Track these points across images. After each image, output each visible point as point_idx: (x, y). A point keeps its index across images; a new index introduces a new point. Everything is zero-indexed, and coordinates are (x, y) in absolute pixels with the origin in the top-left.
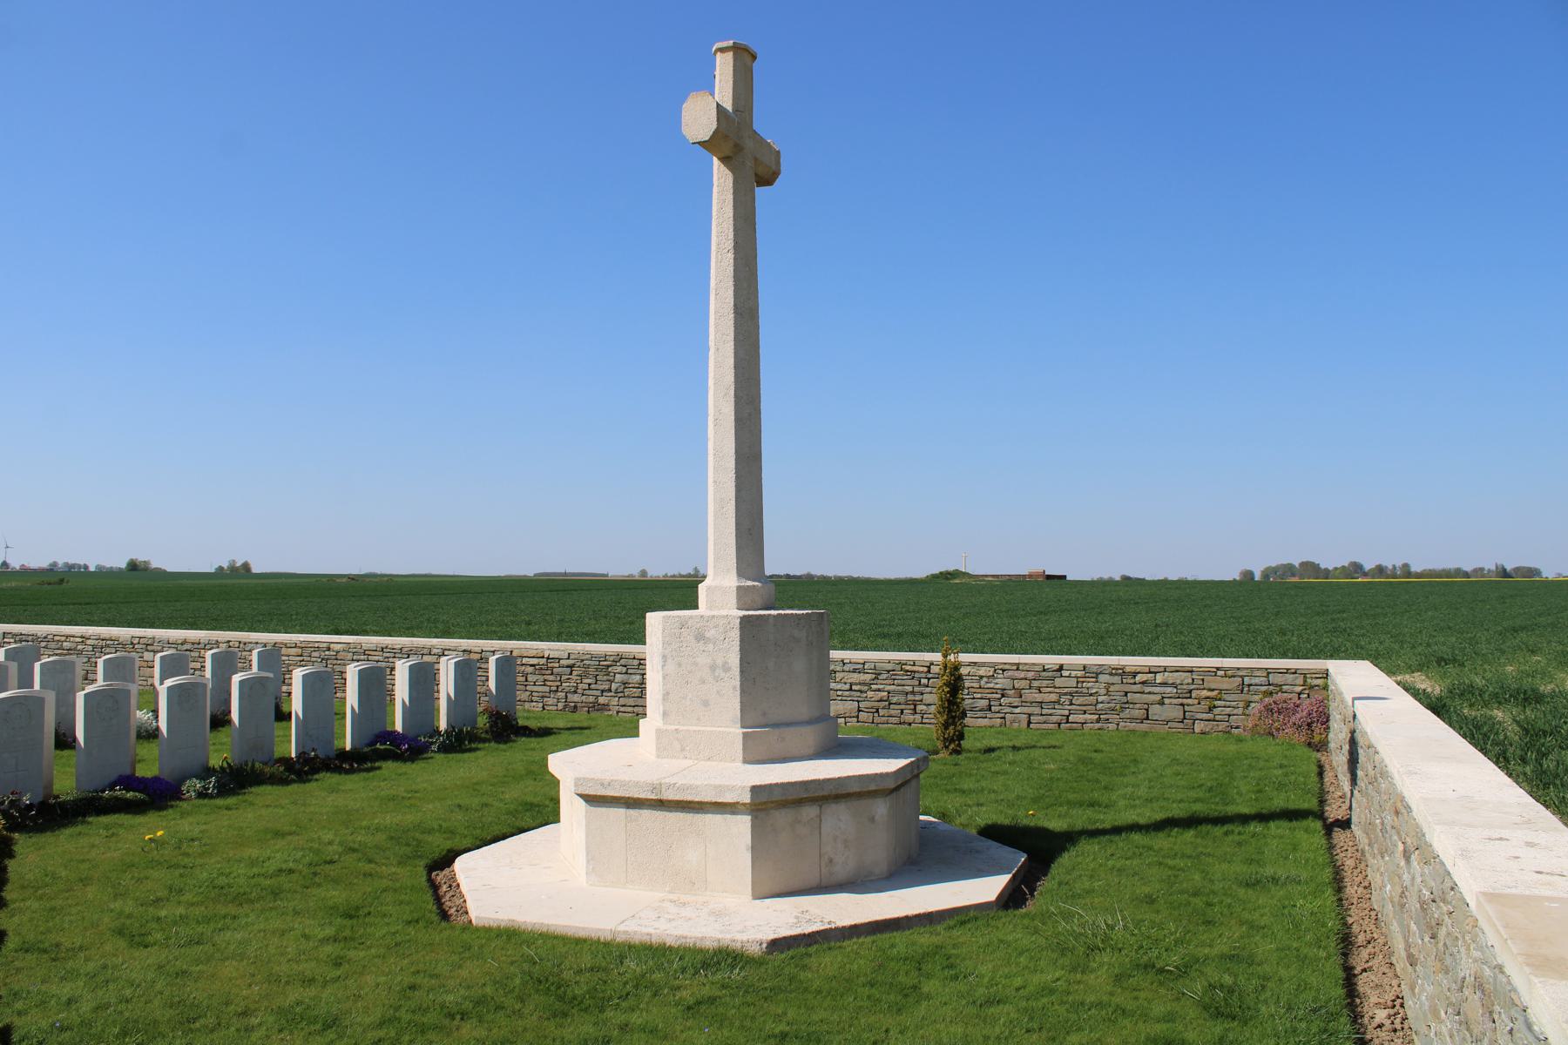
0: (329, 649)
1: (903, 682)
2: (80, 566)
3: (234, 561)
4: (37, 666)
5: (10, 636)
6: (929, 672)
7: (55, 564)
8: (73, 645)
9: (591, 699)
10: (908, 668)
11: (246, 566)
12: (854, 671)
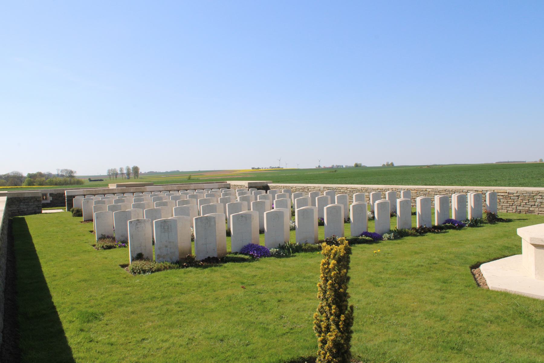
0: (426, 191)
2: (341, 166)
5: (326, 188)
7: (333, 166)
8: (344, 191)
9: (527, 209)
11: (392, 164)
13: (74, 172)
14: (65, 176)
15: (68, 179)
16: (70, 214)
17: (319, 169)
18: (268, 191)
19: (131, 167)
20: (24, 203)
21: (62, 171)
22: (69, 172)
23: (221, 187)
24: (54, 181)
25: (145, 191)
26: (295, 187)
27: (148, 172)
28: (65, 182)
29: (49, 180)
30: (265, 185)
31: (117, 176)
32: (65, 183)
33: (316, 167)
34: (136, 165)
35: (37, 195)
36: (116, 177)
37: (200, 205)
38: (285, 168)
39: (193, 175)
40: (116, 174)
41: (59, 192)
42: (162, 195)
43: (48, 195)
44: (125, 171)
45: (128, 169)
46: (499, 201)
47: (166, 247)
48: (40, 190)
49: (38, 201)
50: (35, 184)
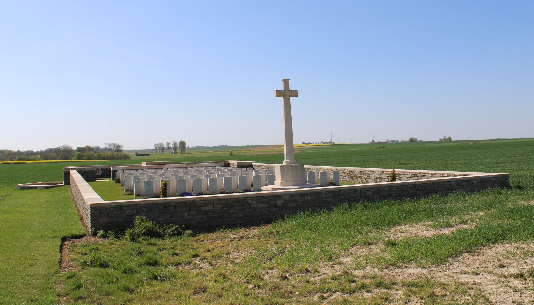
0: (327, 170)
1: (416, 177)
2: (396, 141)
3: (445, 137)
4: (307, 173)
6: (420, 175)
7: (388, 140)
9: (367, 181)
10: (417, 174)
11: (450, 139)
12: (408, 174)
13: (121, 146)
14: (113, 150)
15: (116, 153)
16: (114, 182)
17: (373, 144)
19: (178, 142)
21: (109, 145)
22: (117, 147)
24: (102, 156)
27: (196, 147)
28: (113, 156)
29: (97, 155)
30: (250, 164)
31: (164, 151)
32: (112, 158)
33: (370, 142)
34: (183, 140)
35: (94, 170)
36: (163, 152)
38: (337, 143)
39: (235, 151)
40: (163, 149)
41: (107, 167)
42: (211, 168)
44: (172, 146)
45: (175, 144)
46: (356, 176)
47: (149, 191)
48: (94, 166)
49: (94, 173)
50: (84, 158)
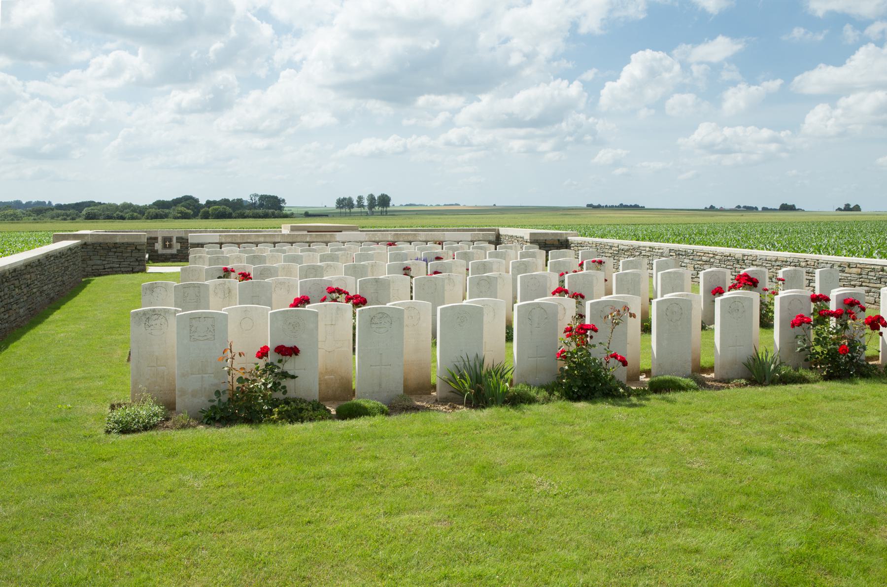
0: (883, 270)
4: (511, 262)
5: (673, 251)
8: (708, 259)
18: (550, 252)
20: (115, 252)
23: (476, 238)
25: (333, 240)
26: (616, 245)
30: (563, 238)
37: (657, 272)
43: (174, 240)
